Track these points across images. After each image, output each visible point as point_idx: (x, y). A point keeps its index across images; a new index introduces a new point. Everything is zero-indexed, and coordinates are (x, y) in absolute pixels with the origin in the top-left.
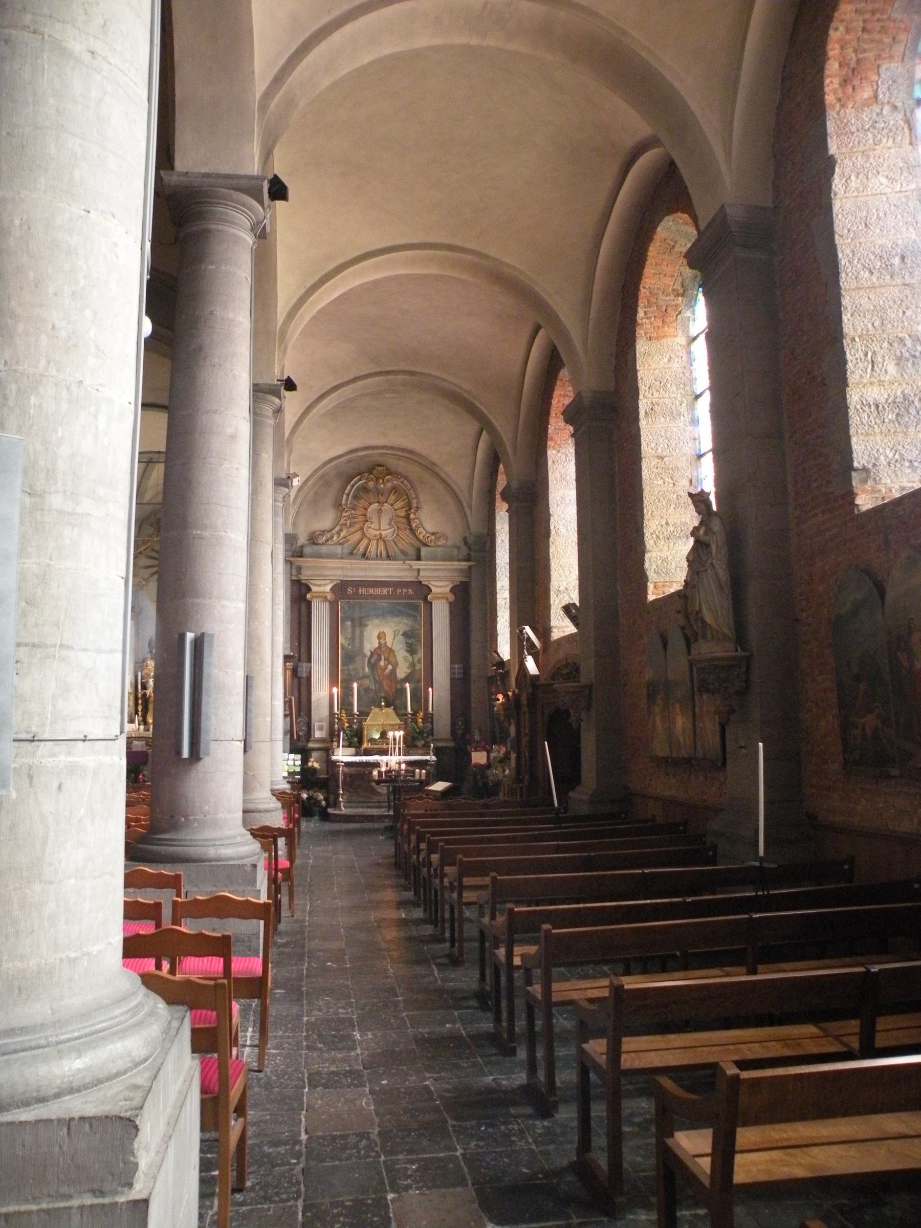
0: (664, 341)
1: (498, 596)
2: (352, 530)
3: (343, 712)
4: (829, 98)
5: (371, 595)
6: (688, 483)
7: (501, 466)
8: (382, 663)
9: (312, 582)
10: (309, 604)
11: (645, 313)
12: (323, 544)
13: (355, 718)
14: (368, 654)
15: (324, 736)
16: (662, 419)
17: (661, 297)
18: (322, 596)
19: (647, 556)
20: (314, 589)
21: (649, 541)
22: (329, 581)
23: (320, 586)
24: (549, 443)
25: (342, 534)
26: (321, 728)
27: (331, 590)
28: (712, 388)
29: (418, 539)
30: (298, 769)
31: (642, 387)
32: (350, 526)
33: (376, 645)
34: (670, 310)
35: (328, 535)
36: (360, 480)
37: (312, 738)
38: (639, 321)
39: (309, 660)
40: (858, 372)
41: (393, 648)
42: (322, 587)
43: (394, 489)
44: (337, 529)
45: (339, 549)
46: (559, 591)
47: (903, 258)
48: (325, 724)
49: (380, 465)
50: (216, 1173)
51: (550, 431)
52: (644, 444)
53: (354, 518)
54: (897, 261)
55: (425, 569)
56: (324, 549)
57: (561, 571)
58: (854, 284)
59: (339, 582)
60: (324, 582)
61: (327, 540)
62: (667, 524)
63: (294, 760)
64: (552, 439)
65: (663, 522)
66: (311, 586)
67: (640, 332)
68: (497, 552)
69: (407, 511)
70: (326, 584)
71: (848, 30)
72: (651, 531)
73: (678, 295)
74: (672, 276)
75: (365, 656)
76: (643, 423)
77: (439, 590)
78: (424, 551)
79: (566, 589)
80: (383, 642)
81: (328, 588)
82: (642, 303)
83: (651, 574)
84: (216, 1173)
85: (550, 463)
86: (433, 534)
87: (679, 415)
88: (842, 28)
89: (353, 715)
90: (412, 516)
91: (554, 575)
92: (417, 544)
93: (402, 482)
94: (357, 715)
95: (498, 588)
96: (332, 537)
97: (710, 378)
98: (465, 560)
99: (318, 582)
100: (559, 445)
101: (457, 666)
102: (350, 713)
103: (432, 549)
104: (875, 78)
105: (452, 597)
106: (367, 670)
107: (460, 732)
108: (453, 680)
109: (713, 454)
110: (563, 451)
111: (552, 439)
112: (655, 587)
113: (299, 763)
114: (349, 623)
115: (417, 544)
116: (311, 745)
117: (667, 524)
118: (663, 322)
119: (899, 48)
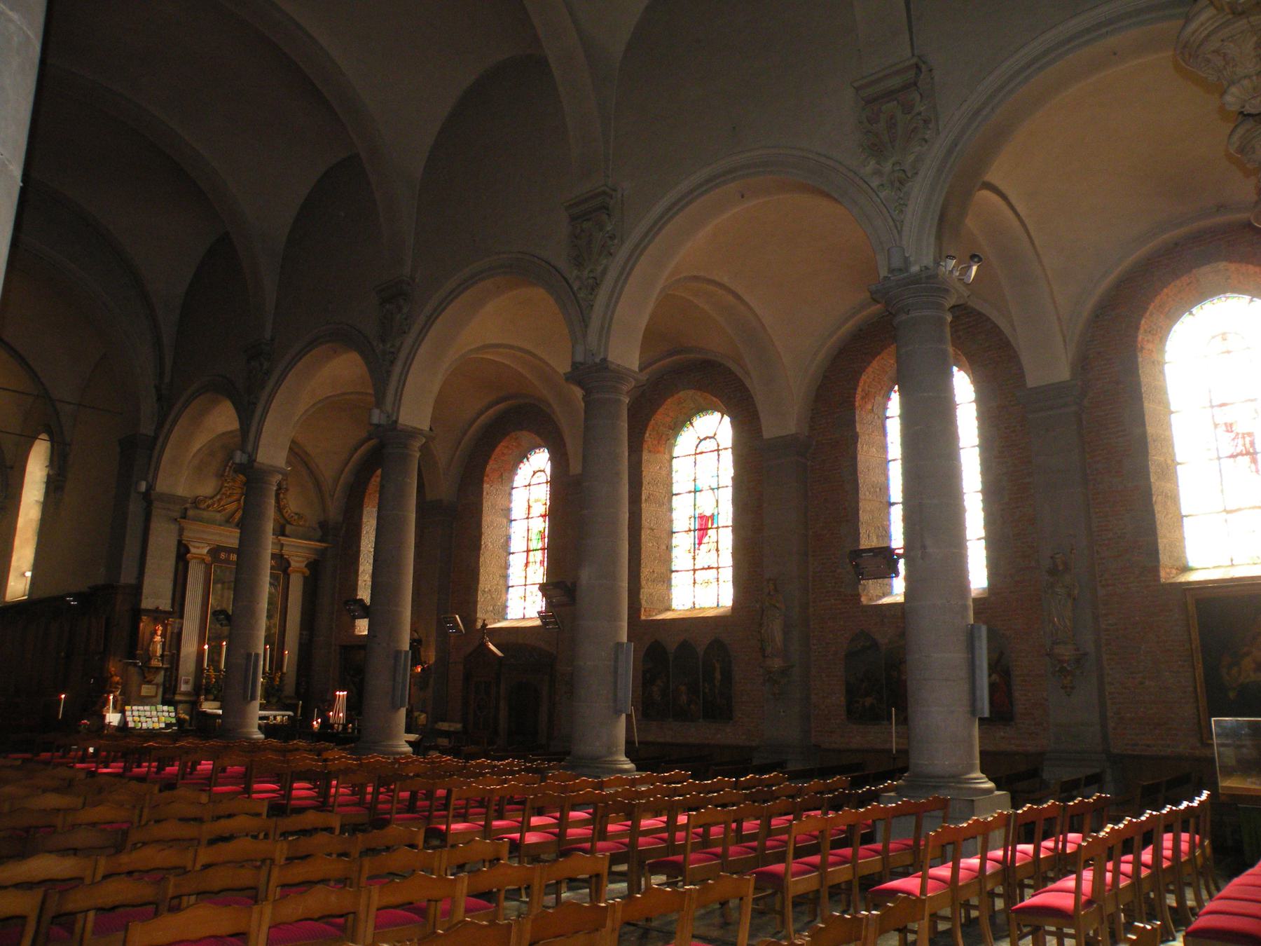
0: (657, 455)
1: (360, 578)
2: (229, 500)
3: (212, 668)
4: (857, 404)
6: (665, 548)
7: (379, 472)
9: (191, 543)
10: (289, 575)
11: (650, 435)
12: (204, 509)
13: (221, 674)
16: (654, 505)
17: (661, 428)
19: (642, 590)
20: (193, 550)
21: (643, 583)
22: (206, 545)
23: (198, 548)
24: (485, 478)
25: (222, 503)
26: (187, 682)
27: (208, 552)
29: (283, 516)
30: (174, 721)
31: (645, 482)
32: (229, 496)
34: (664, 437)
35: (210, 502)
38: (646, 439)
39: (182, 617)
40: (864, 539)
42: (200, 550)
44: (218, 497)
45: (218, 516)
46: (485, 592)
47: (880, 489)
48: (191, 679)
51: (487, 469)
52: (643, 518)
53: (233, 489)
54: (878, 490)
55: (288, 545)
56: (205, 514)
57: (487, 577)
58: (864, 497)
59: (215, 546)
60: (203, 545)
61: (208, 506)
62: (653, 571)
63: (168, 712)
64: (488, 476)
65: (651, 571)
67: (645, 446)
68: (362, 541)
70: (203, 548)
71: (868, 377)
72: (645, 575)
73: (671, 429)
74: (672, 417)
76: (644, 505)
77: (297, 565)
78: (288, 529)
79: (490, 590)
81: (205, 551)
82: (649, 428)
83: (643, 602)
85: (485, 493)
86: (296, 514)
87: (663, 504)
88: (866, 376)
89: (220, 671)
90: (282, 496)
91: (482, 579)
92: (282, 521)
94: (224, 672)
95: (360, 571)
96: (213, 504)
98: (319, 541)
99: (197, 545)
100: (493, 482)
101: (305, 633)
102: (217, 669)
103: (293, 527)
104: (873, 401)
105: (307, 572)
107: (303, 691)
108: (300, 644)
110: (495, 486)
111: (488, 476)
112: (645, 610)
113: (173, 714)
115: (282, 521)
116: (178, 698)
117: (653, 571)
118: (659, 443)
119: (883, 392)
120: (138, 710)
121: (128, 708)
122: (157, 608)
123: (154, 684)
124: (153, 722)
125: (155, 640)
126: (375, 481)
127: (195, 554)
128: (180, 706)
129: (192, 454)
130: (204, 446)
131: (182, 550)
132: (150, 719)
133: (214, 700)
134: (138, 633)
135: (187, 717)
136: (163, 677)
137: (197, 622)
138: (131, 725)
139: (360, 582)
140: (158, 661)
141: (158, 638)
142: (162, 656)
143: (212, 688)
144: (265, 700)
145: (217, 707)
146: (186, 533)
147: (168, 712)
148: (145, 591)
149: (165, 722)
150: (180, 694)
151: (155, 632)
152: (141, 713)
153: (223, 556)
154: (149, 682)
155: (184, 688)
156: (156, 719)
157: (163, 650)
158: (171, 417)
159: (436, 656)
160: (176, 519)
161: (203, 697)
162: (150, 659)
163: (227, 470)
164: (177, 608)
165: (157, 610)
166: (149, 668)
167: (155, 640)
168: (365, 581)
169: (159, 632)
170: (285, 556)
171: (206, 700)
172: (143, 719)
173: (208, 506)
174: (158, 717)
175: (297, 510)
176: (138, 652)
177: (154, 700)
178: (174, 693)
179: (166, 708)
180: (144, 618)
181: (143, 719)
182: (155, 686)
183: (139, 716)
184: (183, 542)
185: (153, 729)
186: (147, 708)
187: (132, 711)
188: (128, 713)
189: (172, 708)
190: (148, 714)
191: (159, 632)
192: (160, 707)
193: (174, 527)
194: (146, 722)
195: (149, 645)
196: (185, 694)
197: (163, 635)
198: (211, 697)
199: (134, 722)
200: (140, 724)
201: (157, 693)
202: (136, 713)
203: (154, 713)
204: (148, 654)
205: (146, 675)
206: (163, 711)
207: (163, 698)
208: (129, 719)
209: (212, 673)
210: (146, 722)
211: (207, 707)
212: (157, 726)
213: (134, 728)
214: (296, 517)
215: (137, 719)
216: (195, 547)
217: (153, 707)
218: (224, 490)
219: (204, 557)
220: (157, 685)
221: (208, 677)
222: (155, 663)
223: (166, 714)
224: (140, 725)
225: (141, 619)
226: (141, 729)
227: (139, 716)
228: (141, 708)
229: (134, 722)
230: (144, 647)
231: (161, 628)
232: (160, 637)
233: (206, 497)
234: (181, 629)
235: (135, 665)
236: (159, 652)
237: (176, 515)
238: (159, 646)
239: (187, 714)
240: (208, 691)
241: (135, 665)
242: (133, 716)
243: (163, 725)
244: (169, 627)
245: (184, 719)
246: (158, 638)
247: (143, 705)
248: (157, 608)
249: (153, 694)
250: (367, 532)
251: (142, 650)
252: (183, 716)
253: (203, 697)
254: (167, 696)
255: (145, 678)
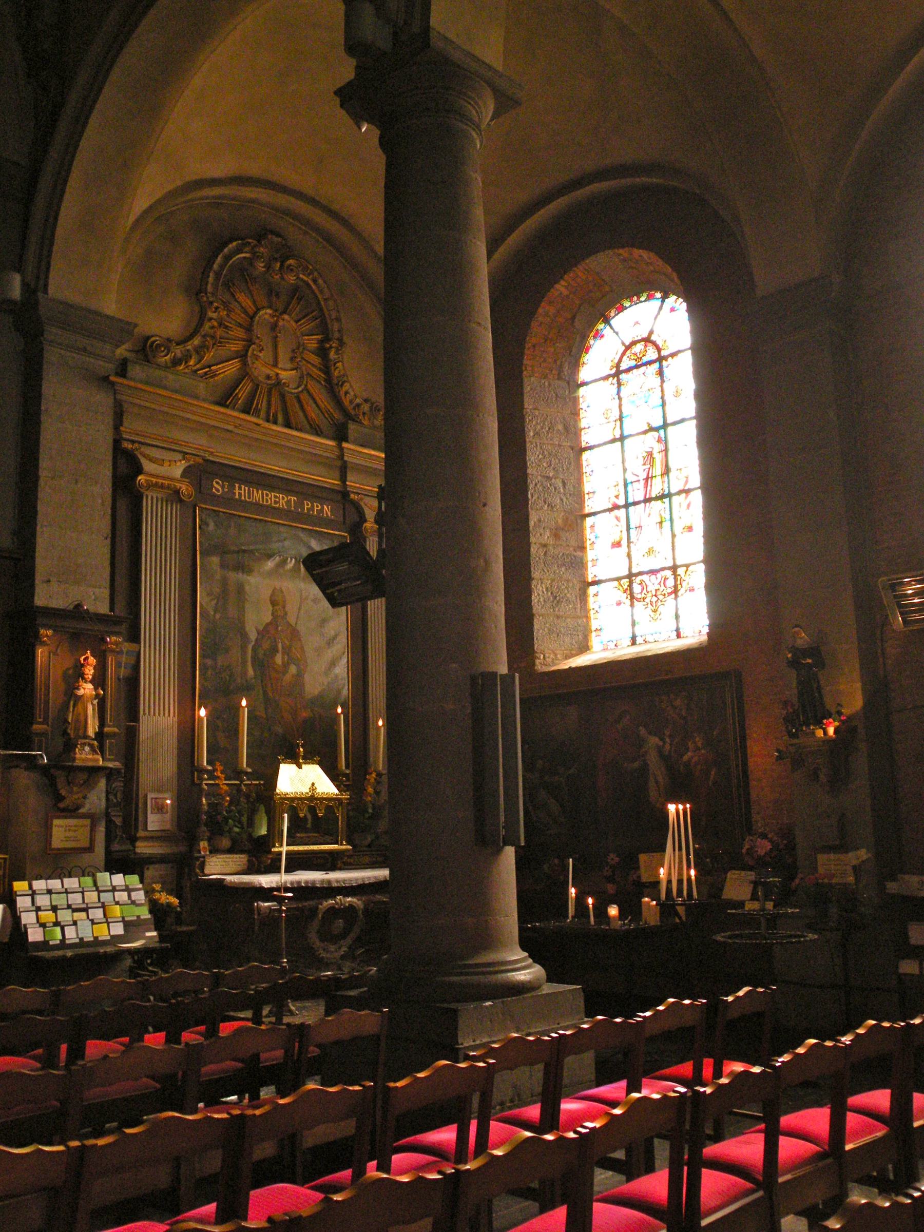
3: (219, 767)
5: (257, 504)
8: (279, 659)
9: (144, 449)
14: (253, 636)
15: (168, 826)
18: (168, 487)
20: (147, 466)
22: (180, 456)
23: (161, 462)
25: (208, 357)
28: (707, 561)
30: (144, 913)
33: (268, 618)
35: (178, 351)
36: (239, 250)
37: (141, 833)
39: (134, 636)
41: (298, 628)
43: (295, 292)
44: (196, 341)
49: (272, 232)
50: (590, 901)
61: (176, 362)
66: (143, 461)
68: (529, 453)
69: (321, 342)
75: (244, 636)
80: (280, 613)
81: (177, 471)
84: (590, 901)
90: (332, 355)
92: (337, 415)
93: (315, 281)
95: (532, 523)
96: (186, 357)
97: (692, 332)
106: (251, 672)
109: (703, 493)
113: (140, 896)
114: (215, 560)
116: (144, 848)
120: (49, 892)
121: (20, 886)
122: (78, 606)
123: (84, 816)
124: (93, 922)
125: (81, 692)
126: (546, 314)
127: (152, 475)
128: (150, 872)
129: (132, 219)
130: (121, 321)
131: (124, 469)
132: (83, 915)
133: (230, 851)
134: (33, 670)
135: (174, 901)
136: (103, 796)
137: (172, 661)
138: (35, 935)
139: (533, 550)
140: (93, 750)
141: (87, 689)
142: (100, 736)
143: (226, 819)
144: (348, 844)
145: (239, 869)
146: (130, 426)
147: (128, 890)
148: (42, 566)
149: (123, 921)
150: (146, 839)
151: (78, 673)
152: (60, 900)
153: (218, 487)
154: (72, 812)
155: (154, 822)
156: (98, 914)
157: (102, 724)
158: (74, 97)
159: (864, 691)
160: (106, 379)
161: (203, 844)
162: (69, 747)
163: (211, 279)
164: (121, 610)
165: (77, 612)
166: (73, 770)
167: (81, 692)
168: (545, 546)
169: (89, 672)
170: (352, 496)
171: (214, 851)
172: (65, 916)
173: (176, 362)
174: (103, 906)
175: (365, 395)
176: (35, 727)
177: (86, 858)
178: (133, 840)
179: (118, 879)
180: (46, 633)
181: (65, 916)
182: (88, 822)
183: (54, 909)
184: (126, 445)
185: (96, 942)
186: (71, 883)
187: (33, 894)
188: (23, 902)
189: (134, 880)
190: (76, 899)
191: (89, 672)
192: (104, 878)
193: (102, 400)
194: (75, 923)
195: (65, 708)
196: (161, 837)
197: (99, 681)
198: (226, 843)
199: (43, 925)
200: (58, 930)
201: (92, 840)
202: (43, 901)
203: (92, 897)
204: (65, 733)
205: (63, 792)
206: (114, 889)
207: (108, 852)
208: (28, 918)
209: (224, 784)
210: (75, 923)
211: (218, 869)
212: (103, 933)
213: (44, 945)
214: (366, 407)
215: (48, 916)
216: (152, 460)
217: (88, 880)
218: (207, 326)
219: (178, 485)
220: (93, 818)
221: (214, 792)
222: (84, 756)
223: (122, 896)
224: (59, 936)
225: (37, 636)
226: (63, 944)
227: (54, 909)
228: (55, 884)
229: (43, 925)
230: (52, 714)
231: (92, 660)
232: (90, 686)
233: (169, 340)
234: (136, 667)
235: (31, 763)
236: (92, 728)
237: (108, 368)
238: (90, 708)
239: (170, 893)
240: (216, 828)
241: (31, 763)
242: (38, 909)
243: (118, 929)
244: (110, 659)
245: (169, 905)
246: (87, 689)
247: (60, 875)
248: (78, 606)
249: (85, 843)
250: (537, 434)
251: (45, 722)
252: (165, 898)
253: (203, 844)
254: (116, 847)
255: (60, 798)
